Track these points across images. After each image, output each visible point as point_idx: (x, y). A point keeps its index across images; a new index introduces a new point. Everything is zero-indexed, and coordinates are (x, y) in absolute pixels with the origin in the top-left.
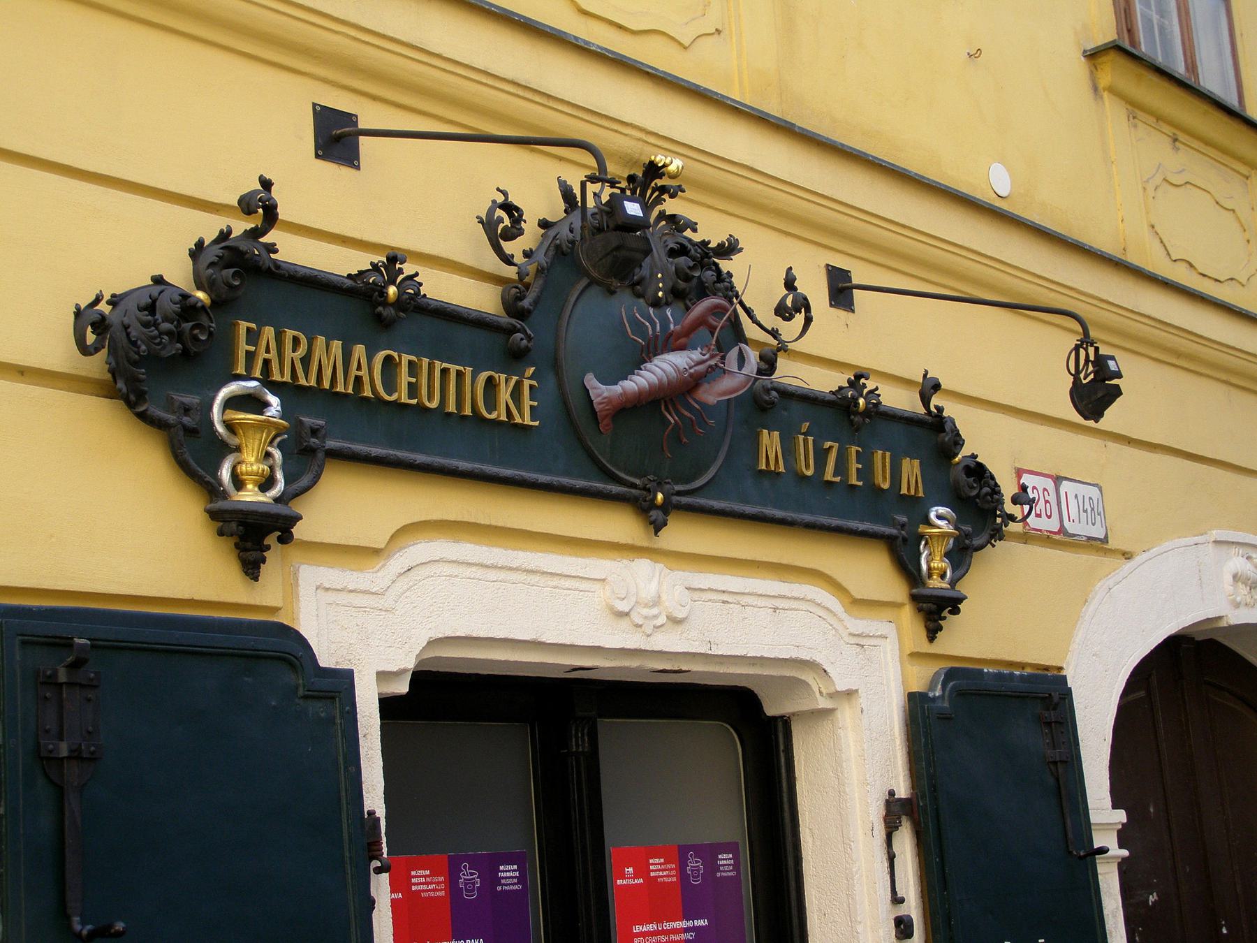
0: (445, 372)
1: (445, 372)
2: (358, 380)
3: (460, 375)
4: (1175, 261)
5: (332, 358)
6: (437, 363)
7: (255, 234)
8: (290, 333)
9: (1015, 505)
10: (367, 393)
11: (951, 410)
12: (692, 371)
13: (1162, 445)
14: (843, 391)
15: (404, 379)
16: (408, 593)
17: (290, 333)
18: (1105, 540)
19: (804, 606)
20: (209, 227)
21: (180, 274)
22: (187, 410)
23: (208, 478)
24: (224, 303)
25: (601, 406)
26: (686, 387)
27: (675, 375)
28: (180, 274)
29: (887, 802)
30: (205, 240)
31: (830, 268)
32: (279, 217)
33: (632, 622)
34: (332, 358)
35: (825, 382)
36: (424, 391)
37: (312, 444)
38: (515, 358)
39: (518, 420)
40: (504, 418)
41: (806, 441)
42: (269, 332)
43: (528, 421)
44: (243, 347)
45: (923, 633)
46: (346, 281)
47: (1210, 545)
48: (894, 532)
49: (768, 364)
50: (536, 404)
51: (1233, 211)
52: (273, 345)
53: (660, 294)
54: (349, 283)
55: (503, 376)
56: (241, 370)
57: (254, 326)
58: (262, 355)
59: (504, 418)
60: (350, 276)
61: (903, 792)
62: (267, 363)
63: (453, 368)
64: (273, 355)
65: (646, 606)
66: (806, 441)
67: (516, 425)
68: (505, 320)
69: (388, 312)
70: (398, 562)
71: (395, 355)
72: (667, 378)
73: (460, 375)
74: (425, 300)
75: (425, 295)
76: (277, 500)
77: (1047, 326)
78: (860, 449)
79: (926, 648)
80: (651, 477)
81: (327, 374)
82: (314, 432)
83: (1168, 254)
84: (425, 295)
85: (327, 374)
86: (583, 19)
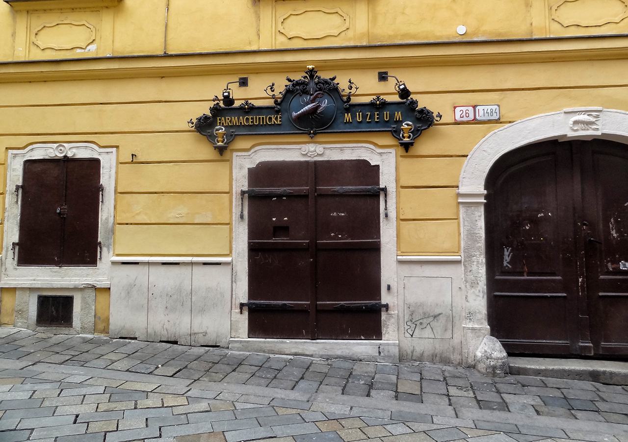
0: (259, 118)
1: (259, 118)
2: (241, 122)
3: (263, 118)
4: (290, 38)
10: (243, 124)
11: (414, 97)
15: (250, 120)
18: (499, 119)
20: (212, 104)
21: (208, 113)
22: (209, 133)
26: (315, 109)
28: (208, 113)
32: (398, 96)
35: (367, 100)
36: (255, 122)
38: (278, 112)
39: (276, 123)
40: (273, 123)
41: (359, 114)
42: (223, 118)
43: (279, 123)
44: (218, 121)
45: (405, 151)
47: (563, 114)
49: (349, 99)
51: (337, 12)
59: (273, 123)
62: (223, 123)
63: (261, 117)
64: (224, 122)
65: (311, 152)
66: (359, 114)
70: (252, 151)
73: (263, 118)
77: (606, 61)
79: (405, 154)
82: (232, 132)
83: (563, 26)
86: (306, 42)
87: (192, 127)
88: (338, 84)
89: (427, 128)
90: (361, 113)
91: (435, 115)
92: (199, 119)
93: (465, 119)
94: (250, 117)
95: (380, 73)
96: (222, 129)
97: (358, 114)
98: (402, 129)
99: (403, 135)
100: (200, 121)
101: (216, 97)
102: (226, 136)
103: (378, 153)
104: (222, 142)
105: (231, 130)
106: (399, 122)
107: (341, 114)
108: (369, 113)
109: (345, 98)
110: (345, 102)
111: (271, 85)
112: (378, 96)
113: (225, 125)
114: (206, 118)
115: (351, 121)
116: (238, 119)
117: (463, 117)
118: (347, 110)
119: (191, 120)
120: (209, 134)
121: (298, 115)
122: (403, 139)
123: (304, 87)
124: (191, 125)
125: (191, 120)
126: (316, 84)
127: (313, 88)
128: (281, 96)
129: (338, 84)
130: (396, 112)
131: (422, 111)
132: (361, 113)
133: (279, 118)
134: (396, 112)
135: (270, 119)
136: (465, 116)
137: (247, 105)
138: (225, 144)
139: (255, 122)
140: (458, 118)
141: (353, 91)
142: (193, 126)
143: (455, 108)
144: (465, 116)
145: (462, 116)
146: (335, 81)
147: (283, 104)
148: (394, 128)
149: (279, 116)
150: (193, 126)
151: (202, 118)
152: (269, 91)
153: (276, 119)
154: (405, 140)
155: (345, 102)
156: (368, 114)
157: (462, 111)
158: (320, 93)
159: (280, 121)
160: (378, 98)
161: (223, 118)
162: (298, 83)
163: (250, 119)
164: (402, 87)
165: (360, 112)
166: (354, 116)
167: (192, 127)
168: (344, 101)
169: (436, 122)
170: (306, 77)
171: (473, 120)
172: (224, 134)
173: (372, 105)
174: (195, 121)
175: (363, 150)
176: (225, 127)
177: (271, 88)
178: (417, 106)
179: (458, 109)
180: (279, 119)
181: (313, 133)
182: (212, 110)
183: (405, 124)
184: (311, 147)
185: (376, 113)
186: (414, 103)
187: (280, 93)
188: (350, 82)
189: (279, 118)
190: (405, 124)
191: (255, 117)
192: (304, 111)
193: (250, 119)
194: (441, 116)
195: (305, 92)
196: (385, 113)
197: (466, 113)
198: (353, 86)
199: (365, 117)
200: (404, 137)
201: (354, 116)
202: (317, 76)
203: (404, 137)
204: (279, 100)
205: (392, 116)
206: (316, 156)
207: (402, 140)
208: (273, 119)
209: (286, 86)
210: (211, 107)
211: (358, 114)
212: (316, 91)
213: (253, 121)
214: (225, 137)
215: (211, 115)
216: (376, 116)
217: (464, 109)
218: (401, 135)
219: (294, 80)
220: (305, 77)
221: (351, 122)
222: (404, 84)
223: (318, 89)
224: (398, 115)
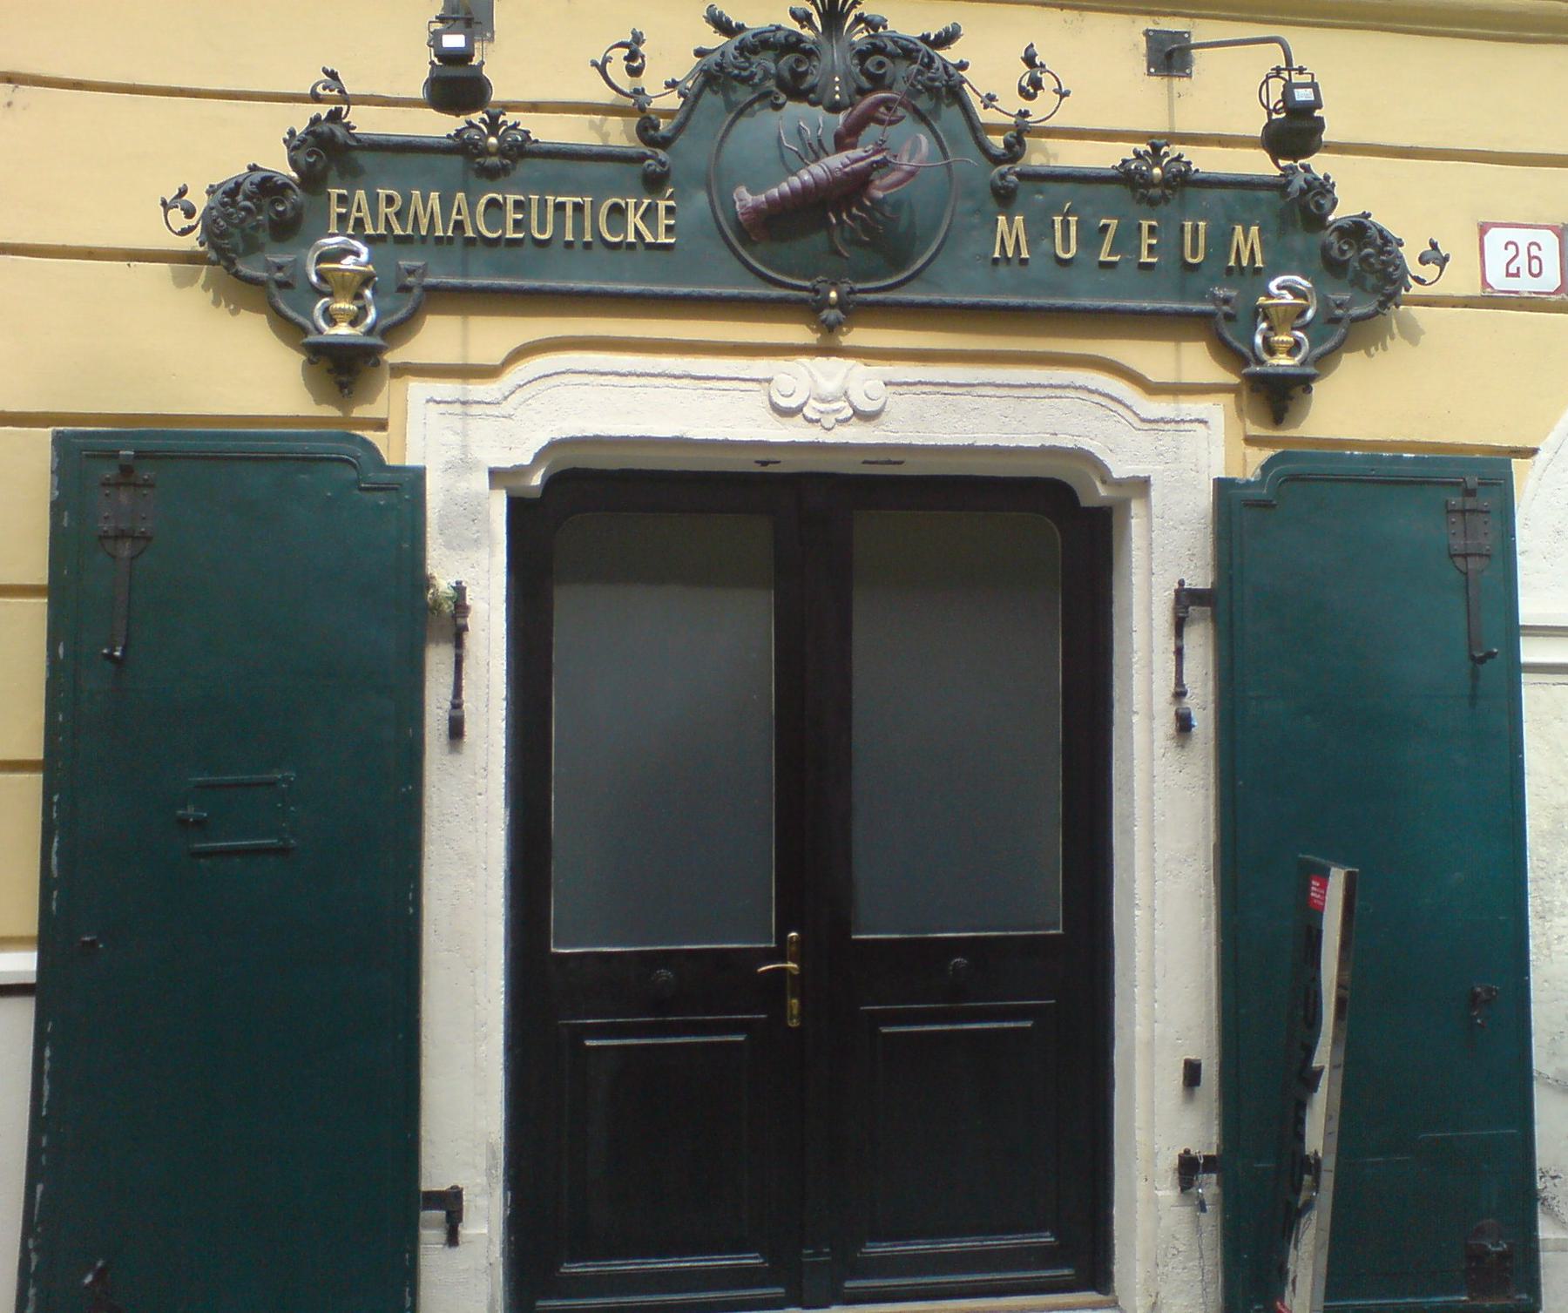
1: (560, 207)
5: (429, 210)
6: (550, 198)
7: (335, 116)
8: (382, 192)
9: (1424, 265)
10: (470, 233)
12: (847, 169)
13: (303, 102)
14: (1127, 164)
15: (512, 216)
16: (530, 401)
17: (382, 192)
19: (1072, 393)
20: (300, 118)
21: (279, 164)
22: (280, 268)
23: (301, 319)
24: (312, 180)
25: (745, 216)
27: (824, 175)
28: (279, 164)
29: (1177, 592)
30: (296, 130)
31: (1151, 33)
33: (805, 417)
34: (429, 210)
35: (1106, 157)
36: (534, 223)
37: (409, 284)
38: (654, 183)
39: (649, 239)
40: (631, 238)
41: (1066, 224)
43: (663, 240)
46: (1280, 179)
48: (1209, 307)
49: (1015, 148)
50: (672, 222)
52: (365, 206)
53: (837, 97)
54: (1114, 172)
55: (632, 201)
56: (333, 229)
57: (344, 192)
58: (355, 214)
59: (631, 238)
60: (449, 136)
61: (1200, 578)
64: (365, 213)
65: (823, 401)
66: (1066, 224)
67: (650, 246)
68: (638, 147)
69: (1155, 192)
71: (500, 198)
72: (814, 179)
73: (578, 208)
74: (1197, 175)
75: (1197, 171)
76: (370, 331)
78: (1154, 223)
80: (820, 278)
81: (424, 222)
82: (411, 272)
84: (1197, 171)
85: (424, 222)
87: (184, 232)
88: (963, 66)
89: (1376, 313)
90: (1073, 219)
91: (1410, 255)
92: (230, 193)
93: (1525, 285)
94: (511, 198)
95: (1153, 38)
96: (357, 254)
97: (1058, 219)
98: (1265, 307)
99: (1266, 340)
100: (234, 203)
101: (333, 75)
102: (374, 292)
103: (1143, 420)
104: (353, 323)
105: (403, 263)
106: (1256, 277)
107: (976, 220)
108: (1114, 223)
109: (997, 142)
110: (997, 160)
111: (629, 38)
112: (1157, 143)
113: (369, 231)
114: (268, 187)
115: (1025, 255)
116: (446, 203)
117: (1517, 275)
118: (1005, 198)
119: (183, 192)
120: (279, 275)
121: (771, 202)
122: (1265, 357)
123: (798, 61)
124: (178, 218)
125: (183, 192)
126: (862, 55)
127: (846, 76)
128: (673, 101)
129: (963, 66)
130: (1239, 229)
131: (1358, 230)
132: (1073, 219)
133: (662, 212)
134: (1239, 229)
135: (617, 211)
136: (1524, 272)
137: (493, 132)
138: (1303, 363)
139: (534, 223)
140: (1498, 281)
141: (1039, 109)
142: (191, 229)
143: (1483, 229)
144: (1524, 272)
145: (1513, 270)
146: (951, 55)
147: (681, 142)
148: (1226, 301)
149: (662, 204)
150: (191, 229)
151: (247, 186)
152: (617, 70)
153: (649, 215)
154: (1275, 361)
155: (997, 160)
156: (1106, 227)
157: (1512, 248)
158: (883, 102)
159: (669, 229)
160: (1156, 148)
161: (361, 194)
162: (765, 43)
163: (510, 206)
164: (1303, 95)
165: (1068, 213)
166: (1039, 231)
167: (184, 232)
168: (994, 151)
169: (1416, 289)
170: (808, 17)
171: (1557, 292)
172: (367, 280)
173: (1125, 178)
174: (199, 200)
175: (1070, 403)
176: (369, 240)
177: (631, 57)
178: (1335, 202)
179: (1495, 238)
180: (663, 221)
181: (841, 305)
182: (294, 144)
183: (1279, 288)
184: (830, 374)
185: (1145, 224)
186: (1322, 189)
187: (672, 85)
188: (1029, 59)
189: (662, 212)
190: (1279, 288)
191: (535, 197)
192: (782, 196)
193: (510, 206)
194: (1446, 259)
195: (796, 89)
196: (1188, 225)
197: (1530, 258)
198: (1047, 81)
199: (1091, 237)
200: (1271, 350)
201: (1039, 231)
202: (860, 19)
203: (1271, 350)
204: (664, 125)
205: (1220, 241)
206: (846, 420)
207: (1261, 362)
208: (634, 220)
209: (700, 53)
210: (292, 133)
211: (1058, 219)
212: (862, 92)
213: (527, 215)
214: (368, 293)
215: (294, 175)
216: (1147, 241)
217: (1523, 237)
218: (1258, 340)
219: (741, 28)
220: (803, 18)
221: (1024, 262)
222: (1314, 86)
223: (866, 84)
224: (1248, 242)
